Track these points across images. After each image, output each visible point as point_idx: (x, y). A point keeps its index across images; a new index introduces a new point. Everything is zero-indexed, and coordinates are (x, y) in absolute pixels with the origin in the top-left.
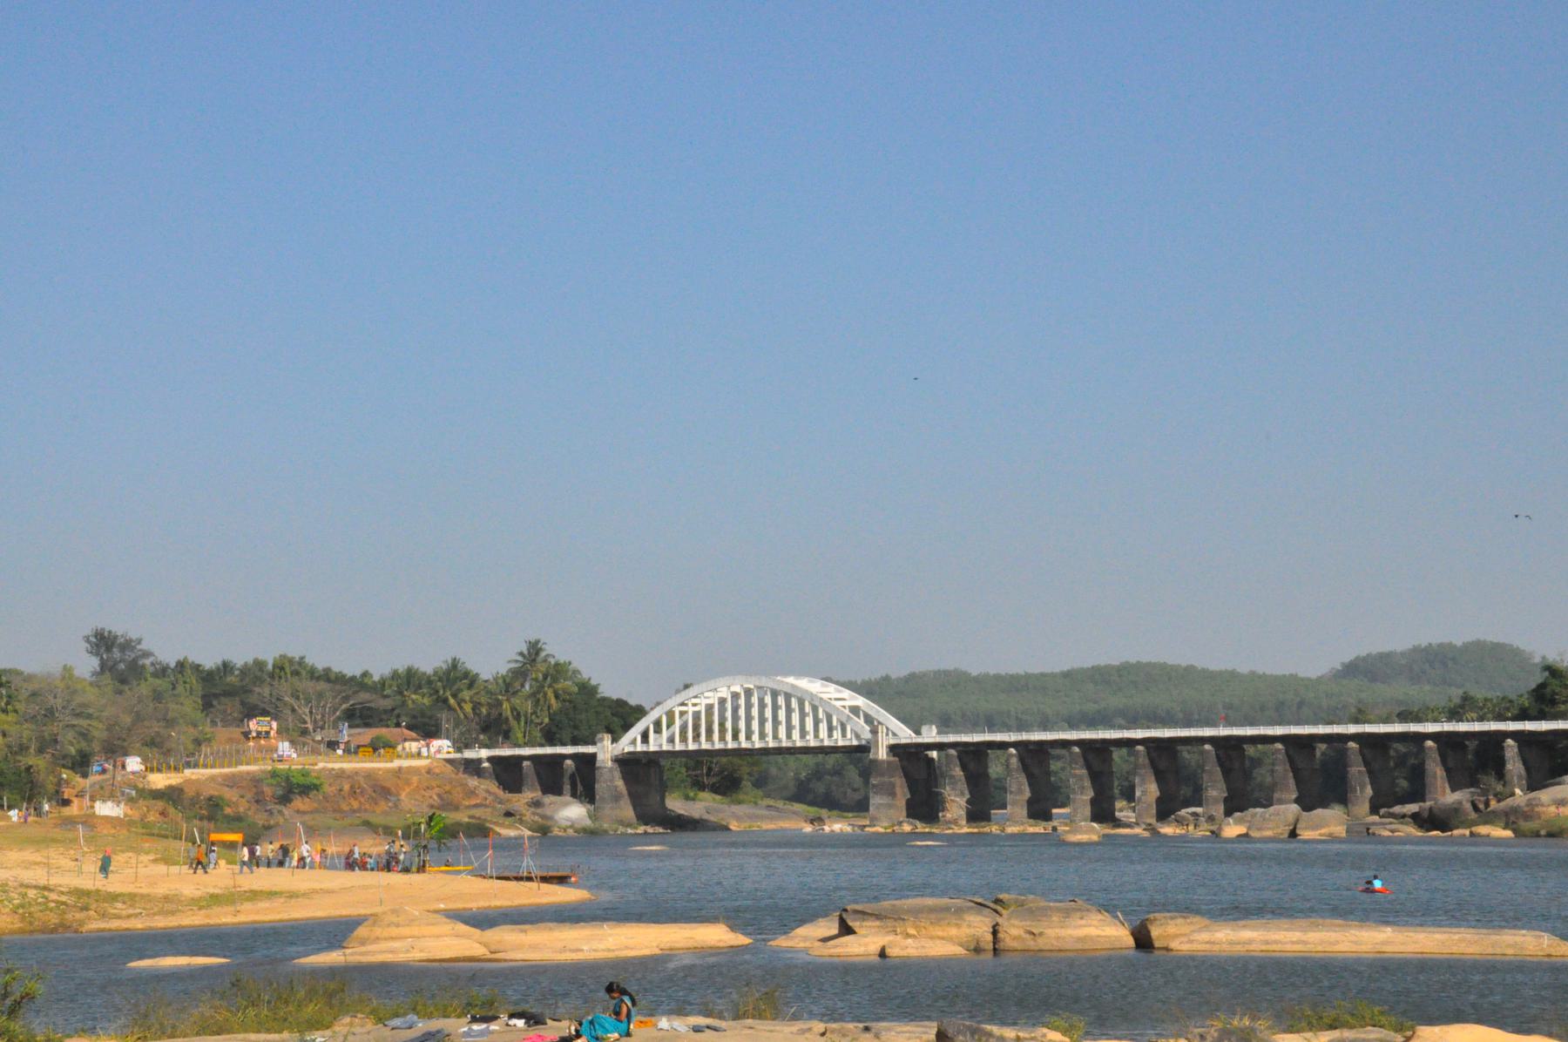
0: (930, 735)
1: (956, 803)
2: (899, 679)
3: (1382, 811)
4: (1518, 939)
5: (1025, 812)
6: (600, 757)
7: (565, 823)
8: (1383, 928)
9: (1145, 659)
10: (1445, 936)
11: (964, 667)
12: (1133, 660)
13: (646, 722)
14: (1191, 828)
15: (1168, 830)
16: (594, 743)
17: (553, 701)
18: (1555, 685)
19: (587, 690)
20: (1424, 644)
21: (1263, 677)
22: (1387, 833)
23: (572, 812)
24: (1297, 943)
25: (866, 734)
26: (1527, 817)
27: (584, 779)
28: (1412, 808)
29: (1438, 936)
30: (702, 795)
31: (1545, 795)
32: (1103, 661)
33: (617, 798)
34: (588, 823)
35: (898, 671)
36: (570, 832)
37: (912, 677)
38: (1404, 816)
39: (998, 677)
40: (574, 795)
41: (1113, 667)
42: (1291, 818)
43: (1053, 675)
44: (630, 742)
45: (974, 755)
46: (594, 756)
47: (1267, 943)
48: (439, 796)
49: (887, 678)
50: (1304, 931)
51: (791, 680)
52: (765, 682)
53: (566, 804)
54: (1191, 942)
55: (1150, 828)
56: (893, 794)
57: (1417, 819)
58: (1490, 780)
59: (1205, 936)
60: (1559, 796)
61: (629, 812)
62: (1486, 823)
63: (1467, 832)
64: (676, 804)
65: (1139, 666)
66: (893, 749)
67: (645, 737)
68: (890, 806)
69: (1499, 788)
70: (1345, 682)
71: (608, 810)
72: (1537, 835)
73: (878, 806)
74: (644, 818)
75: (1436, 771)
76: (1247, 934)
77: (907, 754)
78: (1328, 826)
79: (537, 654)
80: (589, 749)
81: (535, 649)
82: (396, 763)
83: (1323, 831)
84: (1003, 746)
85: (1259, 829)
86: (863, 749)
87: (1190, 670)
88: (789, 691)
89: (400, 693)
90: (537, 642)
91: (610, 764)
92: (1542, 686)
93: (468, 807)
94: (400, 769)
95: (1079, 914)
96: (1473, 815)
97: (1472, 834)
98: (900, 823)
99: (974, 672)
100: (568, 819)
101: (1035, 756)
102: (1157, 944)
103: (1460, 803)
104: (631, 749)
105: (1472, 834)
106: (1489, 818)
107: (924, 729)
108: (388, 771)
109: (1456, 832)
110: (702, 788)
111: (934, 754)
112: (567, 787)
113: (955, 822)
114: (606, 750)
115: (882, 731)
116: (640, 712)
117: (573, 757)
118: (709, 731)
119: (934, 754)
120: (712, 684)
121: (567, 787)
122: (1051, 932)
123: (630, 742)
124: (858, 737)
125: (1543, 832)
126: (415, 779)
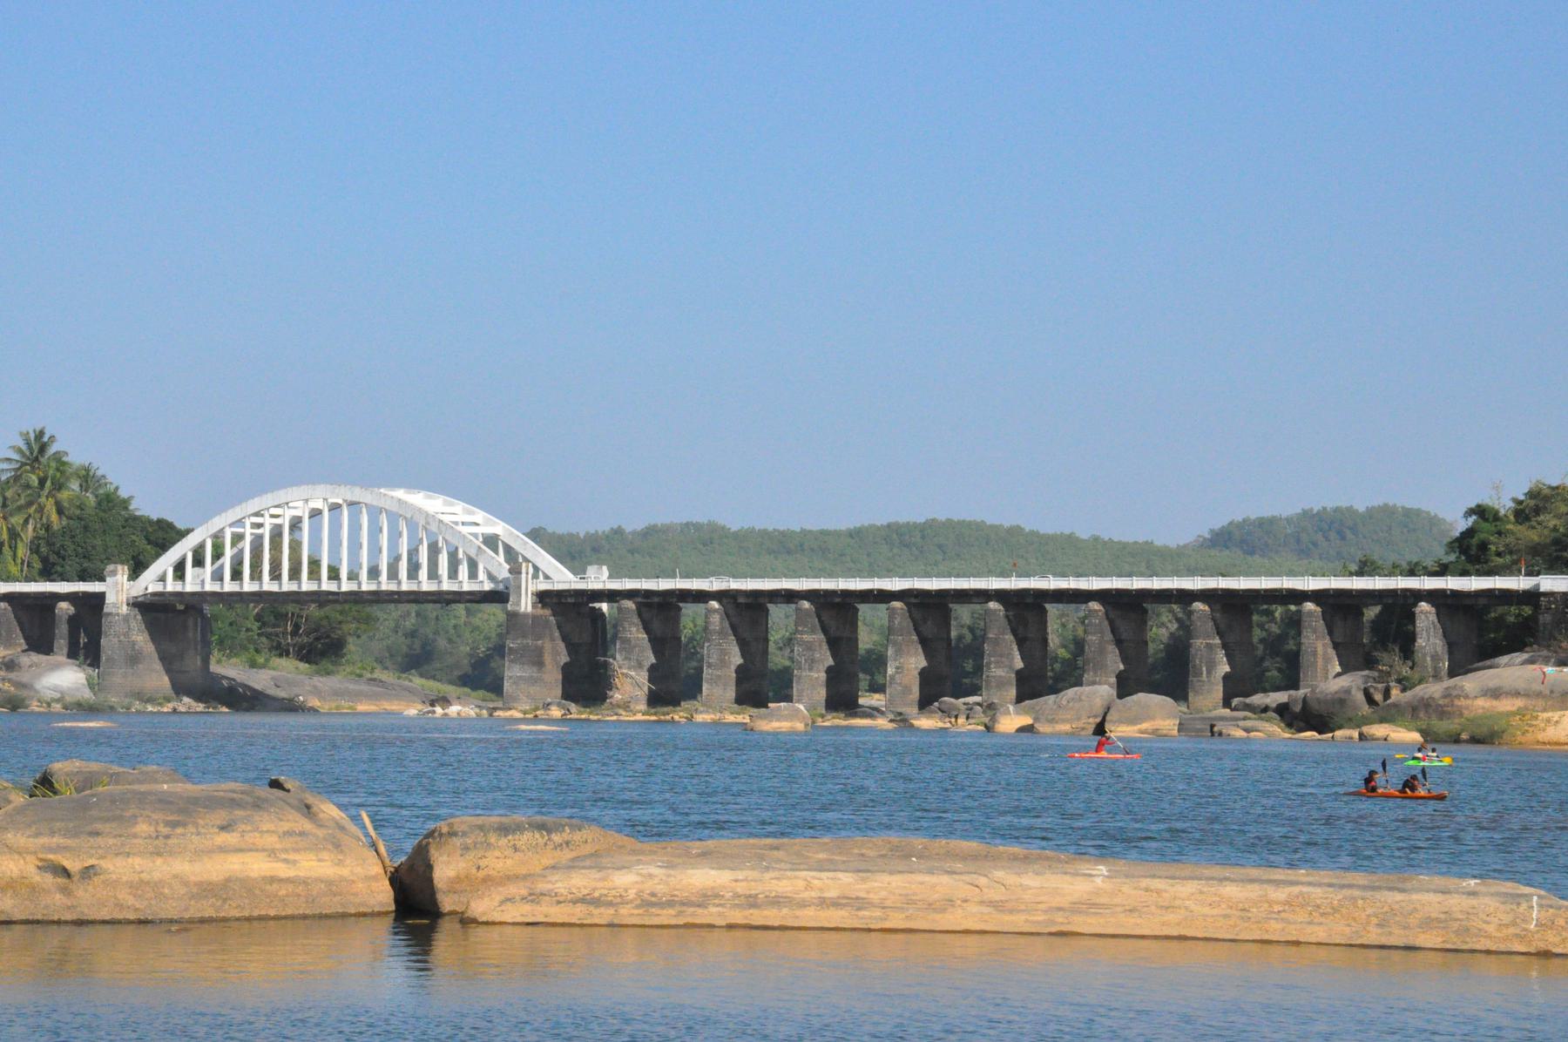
0: (598, 578)
1: (631, 680)
2: (634, 533)
3: (1235, 701)
4: (1457, 903)
5: (731, 693)
6: (110, 599)
7: (49, 695)
8: (1085, 867)
9: (957, 516)
10: (1253, 891)
12: (942, 517)
13: (182, 549)
14: (961, 720)
15: (925, 723)
16: (102, 579)
17: (54, 517)
18: (1486, 532)
19: (111, 503)
22: (1240, 733)
23: (64, 678)
24: (835, 904)
25: (503, 571)
26: (1442, 713)
27: (84, 631)
28: (1281, 697)
29: (1231, 890)
30: (283, 662)
31: (1470, 683)
32: (903, 518)
33: (134, 659)
34: (87, 695)
35: (634, 523)
36: (57, 707)
37: (650, 532)
38: (1265, 709)
39: (764, 534)
40: (72, 655)
41: (915, 525)
42: (1098, 705)
43: (836, 534)
44: (157, 578)
45: (660, 610)
46: (101, 597)
47: (752, 902)
49: (618, 532)
50: (864, 868)
51: (400, 494)
52: (357, 494)
53: (56, 667)
54: (534, 897)
55: (902, 720)
56: (540, 664)
57: (1282, 710)
58: (1391, 660)
59: (581, 882)
60: (1491, 684)
61: (160, 681)
62: (1382, 721)
63: (1356, 734)
64: (229, 669)
65: (950, 525)
66: (543, 597)
67: (179, 570)
68: (533, 681)
69: (1405, 671)
70: (1213, 552)
71: (120, 678)
72: (1457, 741)
73: (517, 681)
74: (180, 689)
75: (1318, 646)
76: (702, 877)
77: (569, 608)
78: (1152, 718)
79: (43, 449)
81: (37, 448)
83: (1144, 726)
84: (701, 597)
85: (1052, 721)
86: (498, 597)
87: (1015, 531)
88: (394, 508)
90: (41, 433)
91: (124, 609)
92: (1469, 533)
95: (221, 816)
96: (1366, 709)
97: (1362, 737)
98: (547, 706)
101: (748, 612)
102: (447, 903)
103: (1348, 691)
104: (159, 588)
105: (1362, 737)
106: (1389, 715)
109: (1338, 733)
110: (283, 652)
111: (604, 607)
112: (61, 643)
113: (626, 706)
114: (119, 589)
115: (526, 571)
117: (71, 597)
119: (604, 607)
120: (281, 496)
121: (61, 643)
122: (121, 868)
123: (157, 578)
124: (491, 577)
125: (1464, 736)
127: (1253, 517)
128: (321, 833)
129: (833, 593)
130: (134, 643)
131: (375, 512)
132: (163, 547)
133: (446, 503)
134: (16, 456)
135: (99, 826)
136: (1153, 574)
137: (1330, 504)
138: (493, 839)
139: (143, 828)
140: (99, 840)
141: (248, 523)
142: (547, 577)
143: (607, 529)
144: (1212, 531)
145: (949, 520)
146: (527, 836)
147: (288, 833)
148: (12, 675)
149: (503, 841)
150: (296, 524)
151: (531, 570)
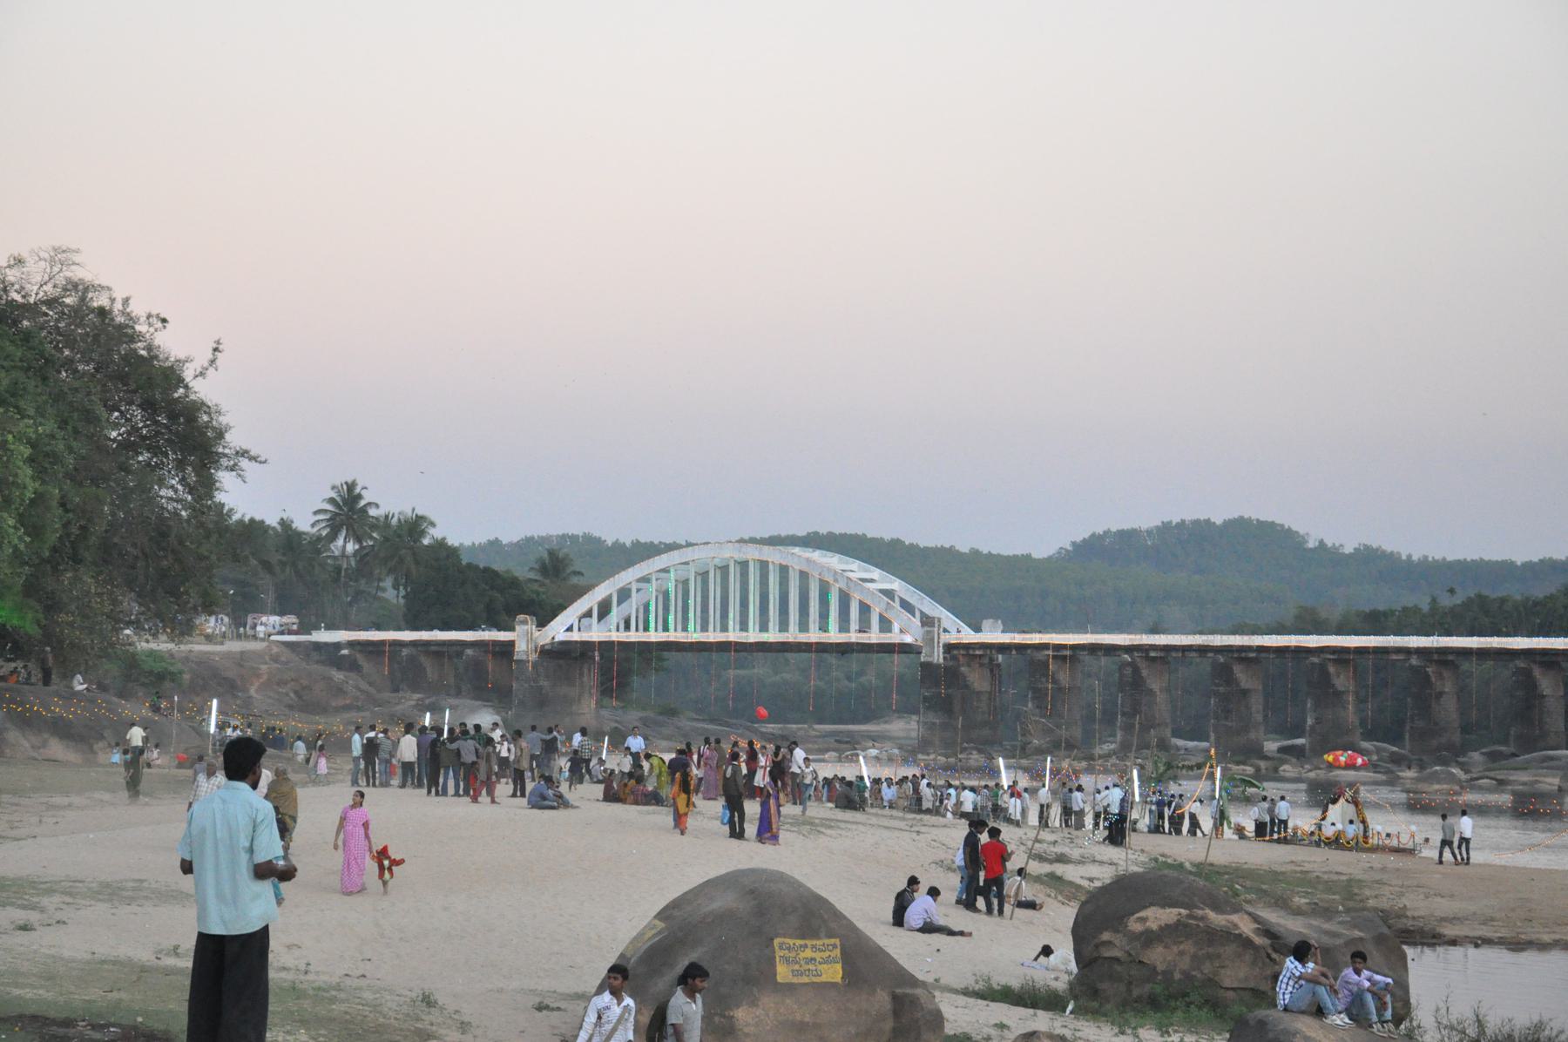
2: (511, 545)
6: (521, 647)
20: (1176, 520)
21: (1489, 563)
37: (1091, 549)
46: (512, 644)
48: (296, 692)
66: (949, 648)
80: (503, 636)
87: (896, 543)
90: (351, 487)
99: (1519, 559)
107: (986, 624)
108: (228, 655)
114: (525, 637)
118: (824, 616)
123: (559, 630)
127: (1114, 529)
129: (1249, 648)
130: (541, 688)
131: (764, 565)
133: (840, 561)
136: (1449, 634)
137: (1189, 516)
144: (1074, 543)
145: (976, 553)
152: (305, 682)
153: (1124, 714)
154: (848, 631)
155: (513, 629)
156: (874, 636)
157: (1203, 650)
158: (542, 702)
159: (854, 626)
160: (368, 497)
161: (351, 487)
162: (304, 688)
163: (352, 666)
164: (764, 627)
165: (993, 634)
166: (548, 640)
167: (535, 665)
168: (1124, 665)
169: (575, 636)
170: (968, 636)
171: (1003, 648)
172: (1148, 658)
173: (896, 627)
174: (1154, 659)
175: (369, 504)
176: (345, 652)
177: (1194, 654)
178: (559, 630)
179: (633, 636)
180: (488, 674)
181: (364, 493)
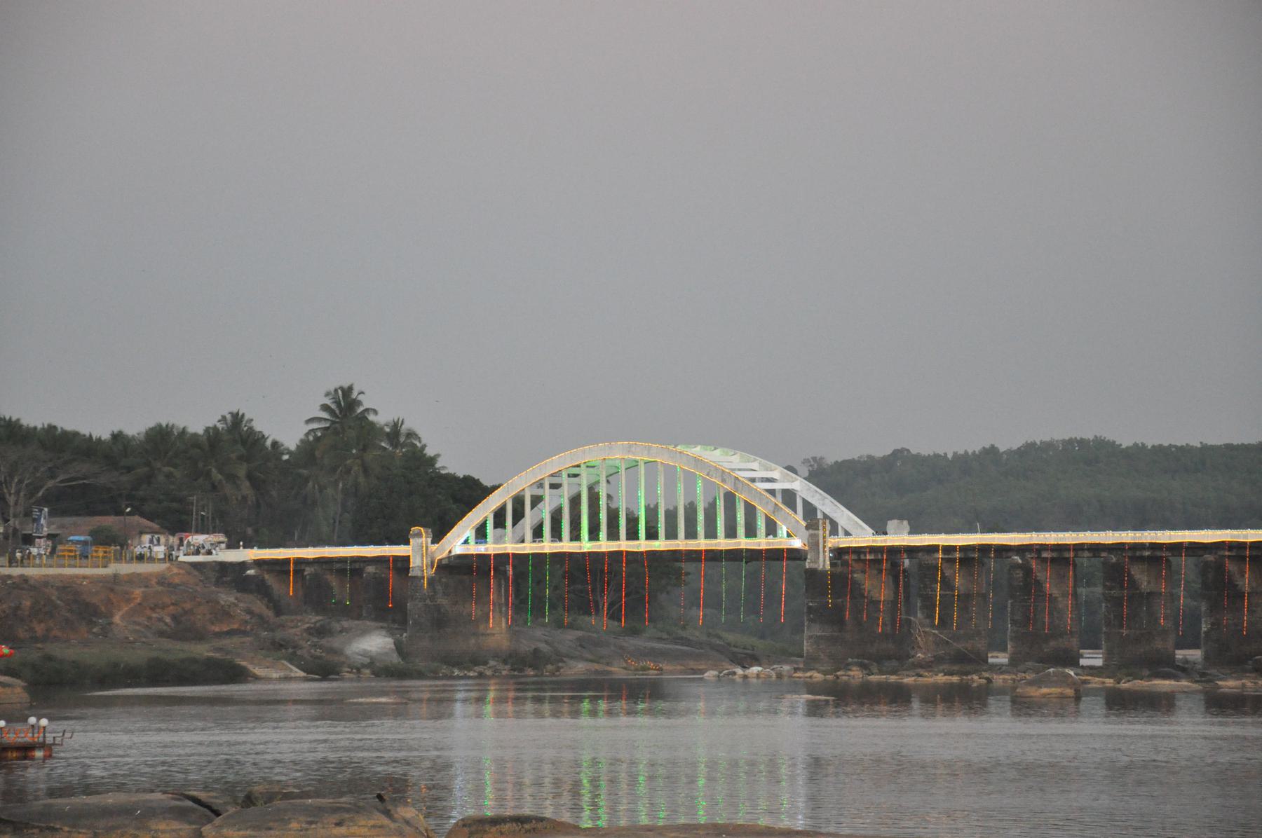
2: (1010, 452)
6: (415, 562)
7: (360, 660)
11: (1109, 436)
13: (484, 511)
19: (419, 461)
34: (395, 659)
37: (1029, 449)
48: (174, 618)
49: (991, 452)
51: (697, 451)
53: (364, 632)
66: (839, 552)
67: (481, 533)
82: (114, 568)
89: (148, 464)
90: (347, 391)
93: (219, 635)
94: (116, 576)
95: (336, 818)
99: (1125, 441)
100: (365, 654)
107: (892, 525)
108: (94, 580)
114: (420, 551)
116: (487, 491)
123: (460, 541)
126: (138, 592)
128: (393, 826)
130: (438, 608)
132: (470, 504)
134: (325, 415)
135: (271, 824)
138: (487, 827)
139: (294, 825)
140: (272, 832)
141: (564, 475)
142: (847, 534)
143: (978, 449)
146: (508, 825)
147: (374, 826)
148: (323, 642)
149: (494, 829)
150: (611, 477)
151: (828, 527)
152: (188, 606)
153: (1014, 622)
154: (637, 538)
155: (407, 543)
156: (761, 542)
157: (1096, 549)
158: (440, 621)
159: (741, 530)
160: (367, 402)
161: (347, 391)
162: (186, 612)
163: (259, 588)
164: (731, 533)
165: (899, 537)
166: (445, 554)
167: (431, 581)
168: (1016, 566)
169: (490, 548)
170: (862, 536)
171: (911, 551)
172: (1039, 557)
173: (783, 530)
174: (1045, 560)
175: (367, 410)
176: (251, 572)
177: (1086, 554)
178: (460, 541)
179: (547, 546)
180: (382, 593)
181: (361, 397)
